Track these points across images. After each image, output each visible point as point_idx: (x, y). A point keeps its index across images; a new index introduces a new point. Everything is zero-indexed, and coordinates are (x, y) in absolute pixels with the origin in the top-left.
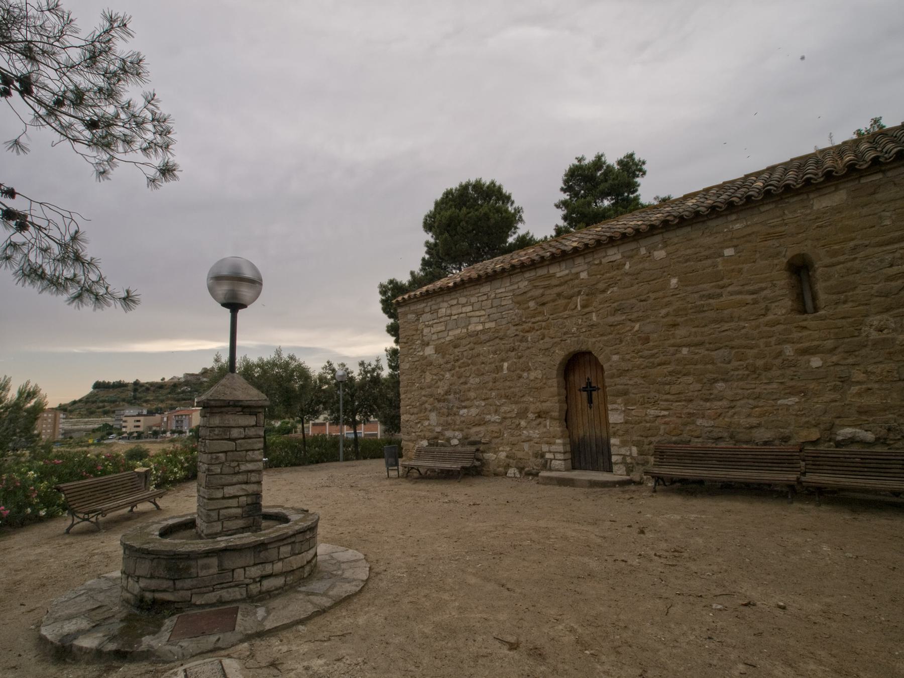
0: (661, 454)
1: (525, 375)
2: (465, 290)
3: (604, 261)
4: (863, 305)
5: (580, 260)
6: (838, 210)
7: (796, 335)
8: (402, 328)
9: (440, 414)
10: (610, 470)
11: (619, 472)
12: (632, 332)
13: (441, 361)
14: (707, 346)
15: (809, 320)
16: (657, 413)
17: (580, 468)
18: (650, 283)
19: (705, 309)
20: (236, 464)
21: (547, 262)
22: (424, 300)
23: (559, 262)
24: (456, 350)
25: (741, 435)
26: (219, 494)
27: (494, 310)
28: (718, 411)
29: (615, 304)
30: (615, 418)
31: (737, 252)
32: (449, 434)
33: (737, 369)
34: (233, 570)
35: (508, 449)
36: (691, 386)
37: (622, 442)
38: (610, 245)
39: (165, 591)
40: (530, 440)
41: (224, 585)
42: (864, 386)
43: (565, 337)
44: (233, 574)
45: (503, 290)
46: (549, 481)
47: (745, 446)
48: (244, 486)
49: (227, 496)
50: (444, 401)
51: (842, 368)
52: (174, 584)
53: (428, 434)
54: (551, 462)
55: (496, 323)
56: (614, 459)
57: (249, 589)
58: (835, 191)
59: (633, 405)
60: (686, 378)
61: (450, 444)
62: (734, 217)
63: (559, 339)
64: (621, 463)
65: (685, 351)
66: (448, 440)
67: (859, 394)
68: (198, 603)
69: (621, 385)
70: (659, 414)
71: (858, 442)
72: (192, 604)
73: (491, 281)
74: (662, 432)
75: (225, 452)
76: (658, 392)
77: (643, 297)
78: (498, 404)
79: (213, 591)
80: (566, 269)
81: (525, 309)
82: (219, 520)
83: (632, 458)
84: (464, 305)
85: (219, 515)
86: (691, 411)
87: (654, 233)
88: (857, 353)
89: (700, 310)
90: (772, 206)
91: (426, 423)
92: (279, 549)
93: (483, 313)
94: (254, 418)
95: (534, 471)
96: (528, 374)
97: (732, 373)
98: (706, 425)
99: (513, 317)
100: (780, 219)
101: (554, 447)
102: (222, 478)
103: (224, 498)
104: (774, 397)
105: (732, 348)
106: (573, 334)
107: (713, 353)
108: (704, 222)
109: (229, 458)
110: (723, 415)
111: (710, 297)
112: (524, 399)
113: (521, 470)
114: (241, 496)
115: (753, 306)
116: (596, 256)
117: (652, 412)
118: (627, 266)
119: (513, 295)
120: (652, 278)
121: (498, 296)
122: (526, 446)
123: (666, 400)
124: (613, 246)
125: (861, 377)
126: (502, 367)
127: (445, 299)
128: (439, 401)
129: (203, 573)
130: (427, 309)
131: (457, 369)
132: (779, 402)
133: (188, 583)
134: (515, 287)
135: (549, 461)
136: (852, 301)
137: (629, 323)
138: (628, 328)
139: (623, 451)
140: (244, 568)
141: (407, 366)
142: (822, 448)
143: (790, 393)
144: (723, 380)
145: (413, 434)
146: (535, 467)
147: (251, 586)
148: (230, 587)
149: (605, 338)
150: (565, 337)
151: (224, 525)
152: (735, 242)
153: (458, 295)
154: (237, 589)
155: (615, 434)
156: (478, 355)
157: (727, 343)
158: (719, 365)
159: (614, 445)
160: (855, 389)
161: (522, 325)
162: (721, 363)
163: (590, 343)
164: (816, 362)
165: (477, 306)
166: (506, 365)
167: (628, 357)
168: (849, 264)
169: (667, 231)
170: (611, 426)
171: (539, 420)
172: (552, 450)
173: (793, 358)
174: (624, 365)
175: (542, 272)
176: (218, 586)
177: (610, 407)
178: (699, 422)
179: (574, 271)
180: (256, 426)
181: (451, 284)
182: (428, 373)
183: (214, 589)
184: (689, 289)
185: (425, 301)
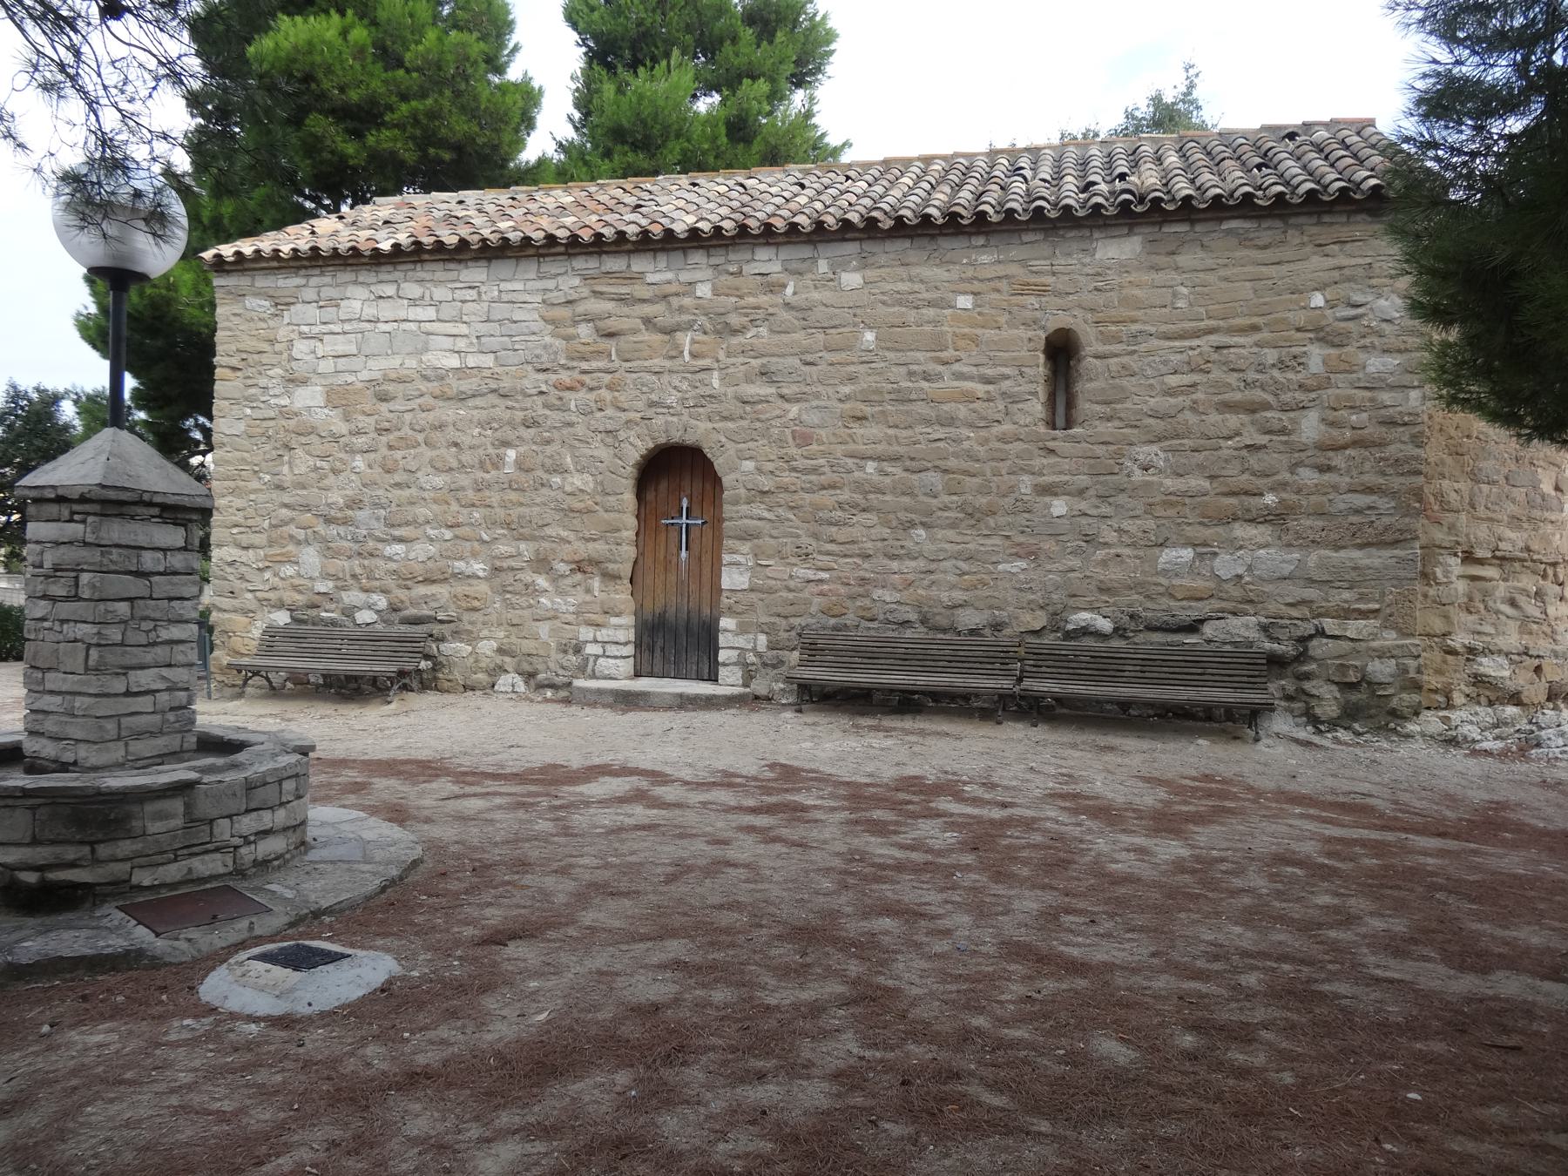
0: (812, 649)
1: (556, 480)
2: (419, 265)
3: (747, 269)
4: (1131, 427)
5: (698, 257)
6: (1124, 268)
7: (1038, 462)
8: (224, 329)
9: (329, 551)
10: (713, 678)
11: (730, 681)
12: (784, 419)
13: (341, 427)
14: (908, 463)
15: (1059, 440)
16: (810, 574)
17: (651, 675)
18: (828, 331)
19: (913, 396)
20: (151, 625)
21: (629, 247)
22: (299, 268)
23: (655, 251)
24: (384, 407)
25: (938, 618)
26: (119, 685)
27: (493, 328)
28: (908, 576)
29: (759, 361)
30: (733, 579)
31: (976, 305)
32: (352, 597)
33: (946, 508)
34: (211, 821)
35: (502, 634)
36: (873, 531)
37: (740, 625)
38: (762, 240)
39: (73, 865)
40: (555, 618)
41: (195, 849)
42: (1113, 551)
43: (650, 413)
44: (211, 829)
45: (519, 286)
46: (594, 700)
47: (941, 636)
48: (165, 672)
49: (135, 690)
50: (346, 522)
51: (1090, 520)
52: (93, 851)
53: (291, 597)
54: (595, 662)
55: (496, 358)
56: (723, 656)
57: (238, 856)
58: (1128, 235)
59: (769, 557)
60: (866, 515)
61: (354, 620)
62: (980, 241)
63: (639, 415)
64: (735, 664)
65: (871, 467)
66: (349, 612)
67: (1104, 563)
68: (146, 883)
69: (752, 518)
70: (812, 577)
71: (1091, 633)
72: (132, 887)
73: (489, 259)
74: (813, 609)
75: (130, 599)
76: (816, 536)
77: (809, 358)
78: (485, 537)
79: (175, 860)
80: (668, 268)
81: (568, 338)
82: (119, 739)
83: (759, 655)
84: (414, 302)
85: (119, 728)
86: (867, 575)
87: (847, 236)
88: (1111, 500)
89: (903, 399)
90: (1039, 236)
91: (289, 570)
92: (280, 785)
93: (463, 329)
94: (182, 530)
95: (559, 680)
96: (564, 479)
97: (940, 513)
98: (888, 600)
99: (538, 352)
100: (1048, 262)
101: (604, 631)
102: (126, 652)
103: (128, 694)
104: (994, 559)
105: (945, 471)
106: (669, 407)
107: (915, 477)
108: (933, 237)
109: (138, 613)
110: (917, 583)
111: (927, 377)
112: (548, 531)
113: (529, 676)
114: (158, 691)
115: (986, 404)
116: (732, 257)
117: (803, 572)
118: (789, 290)
119: (544, 301)
120: (833, 323)
121: (505, 297)
122: (544, 630)
123: (828, 553)
124: (768, 244)
125: (1112, 537)
126: (501, 458)
127: (361, 279)
128: (329, 521)
129: (154, 827)
130: (310, 294)
131: (384, 451)
132: (1000, 567)
133: (126, 847)
134: (551, 284)
135: (591, 659)
136: (1120, 418)
137: (780, 402)
138: (778, 412)
139: (741, 641)
140: (230, 817)
141: (240, 427)
142: (1046, 642)
143: (1016, 554)
144: (923, 524)
145: (249, 596)
146: (561, 672)
147: (243, 851)
148: (207, 852)
149: (730, 425)
150: (650, 413)
151: (131, 749)
152: (977, 286)
153: (398, 275)
154: (218, 856)
155: (731, 611)
156: (441, 427)
157: (938, 463)
158: (922, 498)
159: (726, 630)
160: (1100, 554)
161: (555, 372)
162: (925, 494)
163: (699, 431)
164: (1059, 507)
165: (448, 311)
166: (511, 454)
167: (770, 466)
168: (1125, 360)
169: (869, 238)
170: (724, 594)
171: (579, 576)
172: (599, 639)
173: (1029, 498)
174: (766, 483)
175: (614, 264)
176: (185, 851)
177: (726, 558)
178: (877, 593)
179: (685, 277)
180: (185, 549)
181: (386, 246)
182: (299, 452)
183: (176, 856)
184: (890, 355)
185: (303, 272)
